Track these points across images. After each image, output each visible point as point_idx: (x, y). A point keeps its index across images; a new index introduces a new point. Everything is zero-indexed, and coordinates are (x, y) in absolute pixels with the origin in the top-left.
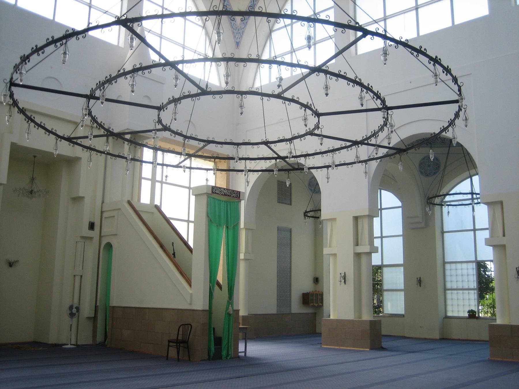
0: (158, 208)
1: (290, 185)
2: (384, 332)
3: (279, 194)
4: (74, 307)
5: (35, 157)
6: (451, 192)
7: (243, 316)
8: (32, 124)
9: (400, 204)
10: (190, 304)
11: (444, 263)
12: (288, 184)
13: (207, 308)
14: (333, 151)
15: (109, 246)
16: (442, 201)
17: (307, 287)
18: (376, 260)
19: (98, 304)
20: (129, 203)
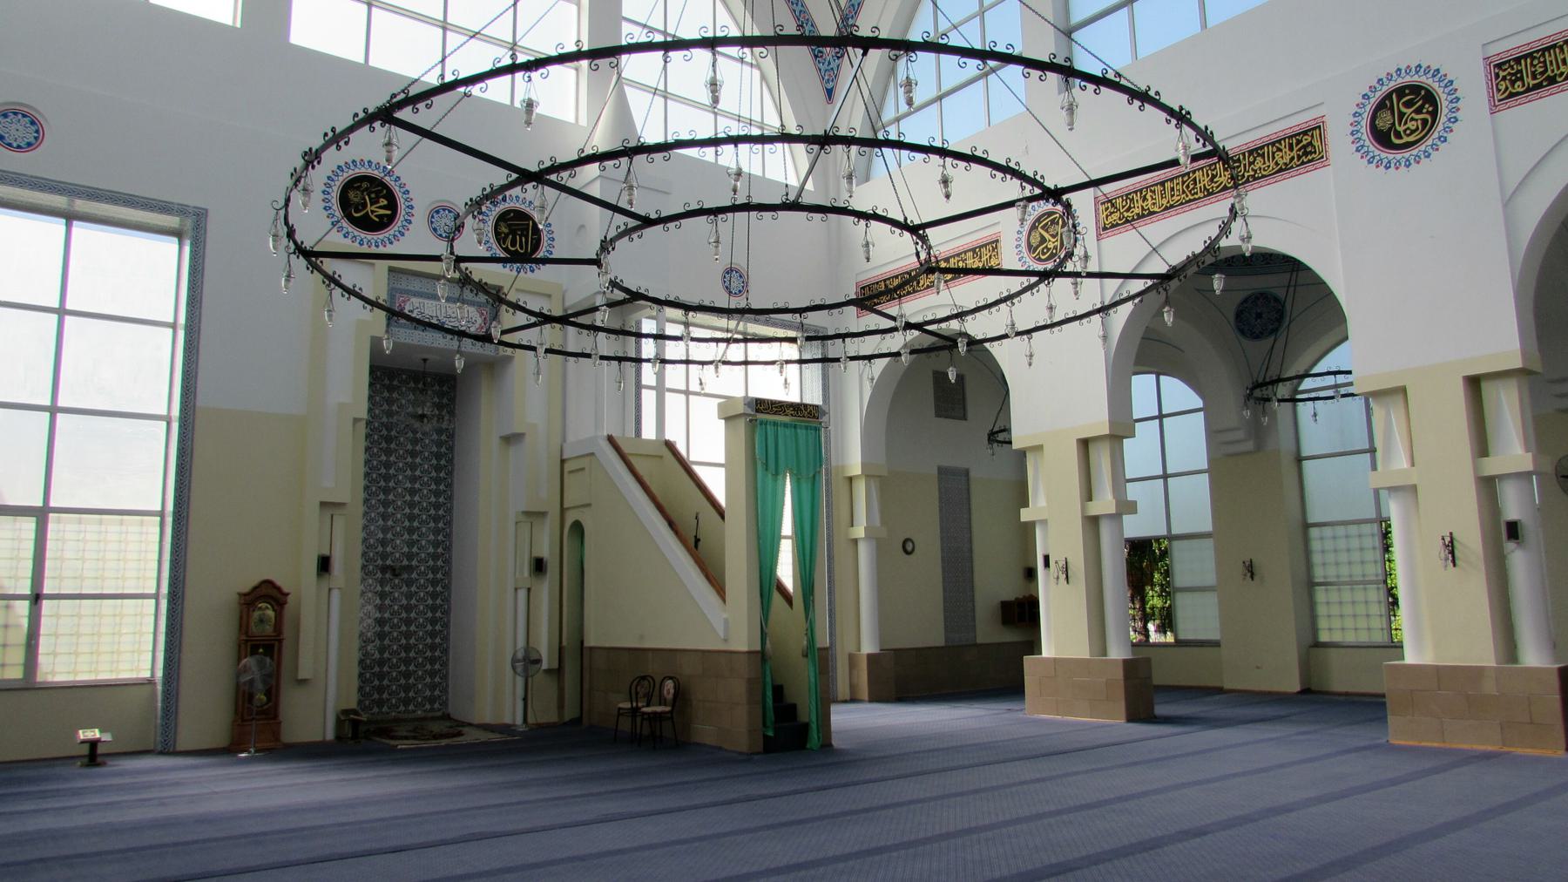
0: (670, 446)
1: (960, 378)
2: (1158, 680)
3: (937, 399)
4: (378, 615)
5: (425, 360)
6: (1315, 370)
7: (870, 656)
8: (338, 291)
9: (1199, 403)
10: (726, 641)
11: (1307, 526)
12: (952, 376)
13: (758, 648)
14: (1009, 298)
15: (578, 528)
16: (1296, 392)
17: (1011, 590)
18: (1135, 527)
19: (565, 643)
20: (610, 439)
